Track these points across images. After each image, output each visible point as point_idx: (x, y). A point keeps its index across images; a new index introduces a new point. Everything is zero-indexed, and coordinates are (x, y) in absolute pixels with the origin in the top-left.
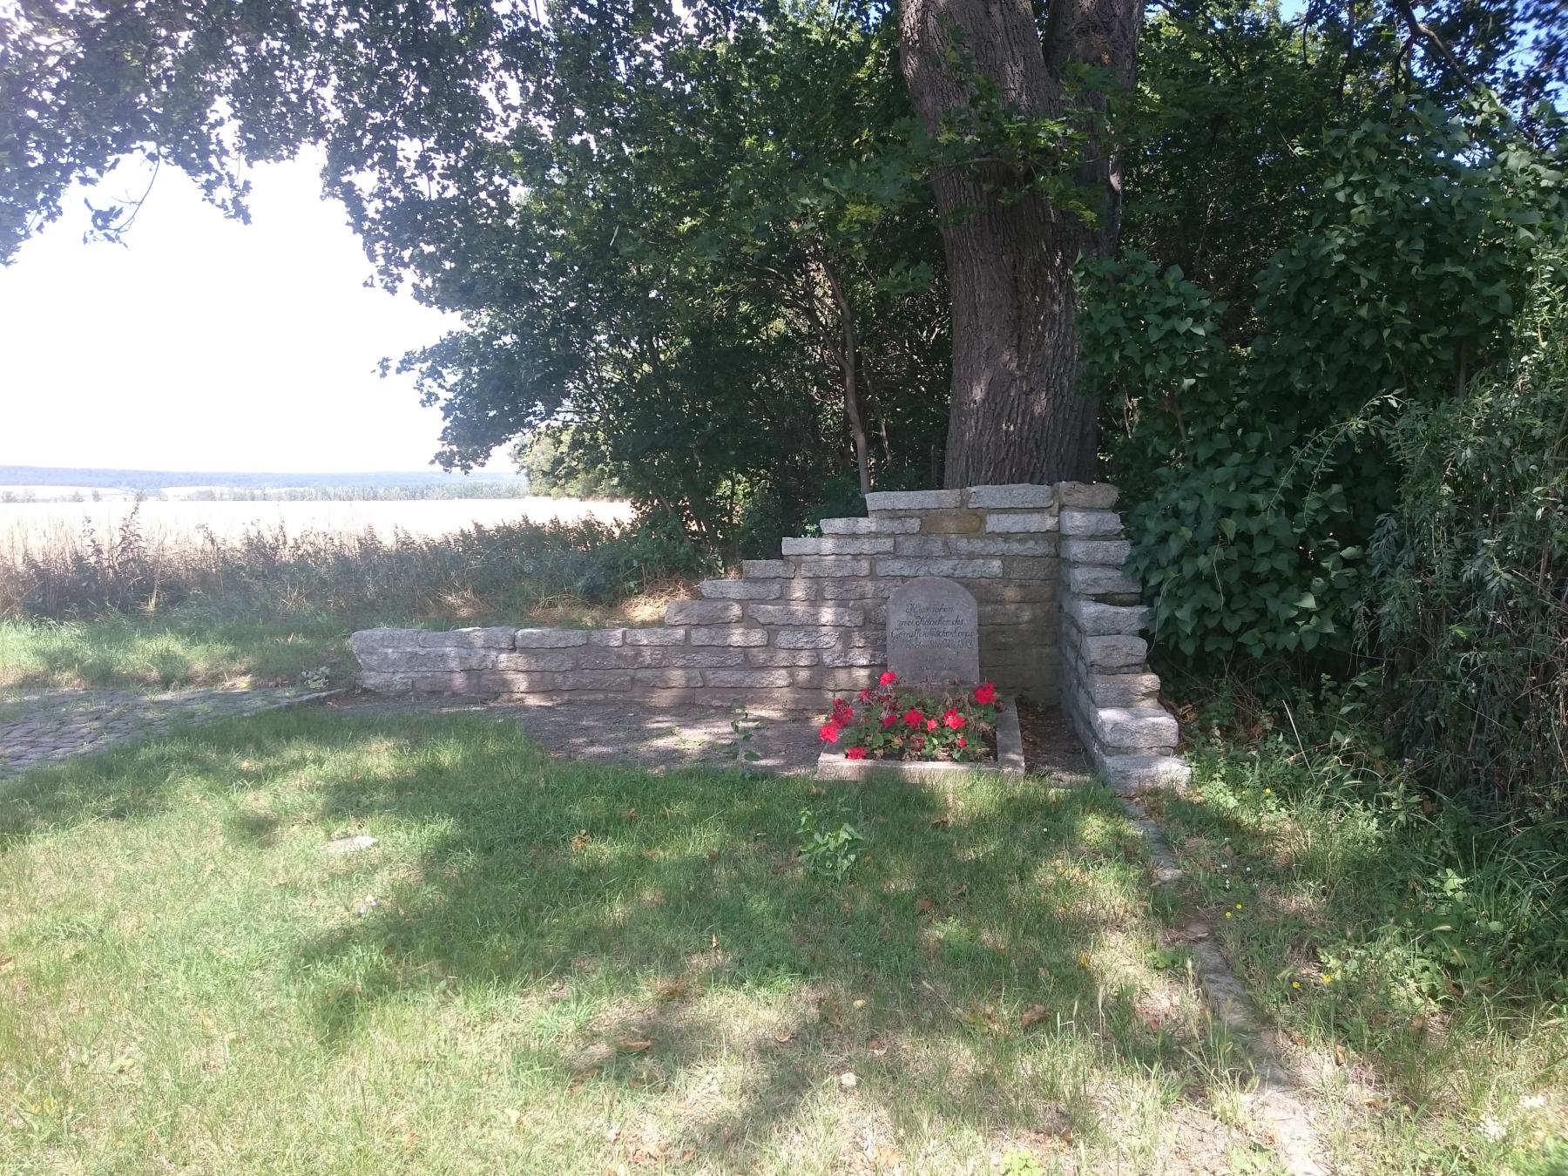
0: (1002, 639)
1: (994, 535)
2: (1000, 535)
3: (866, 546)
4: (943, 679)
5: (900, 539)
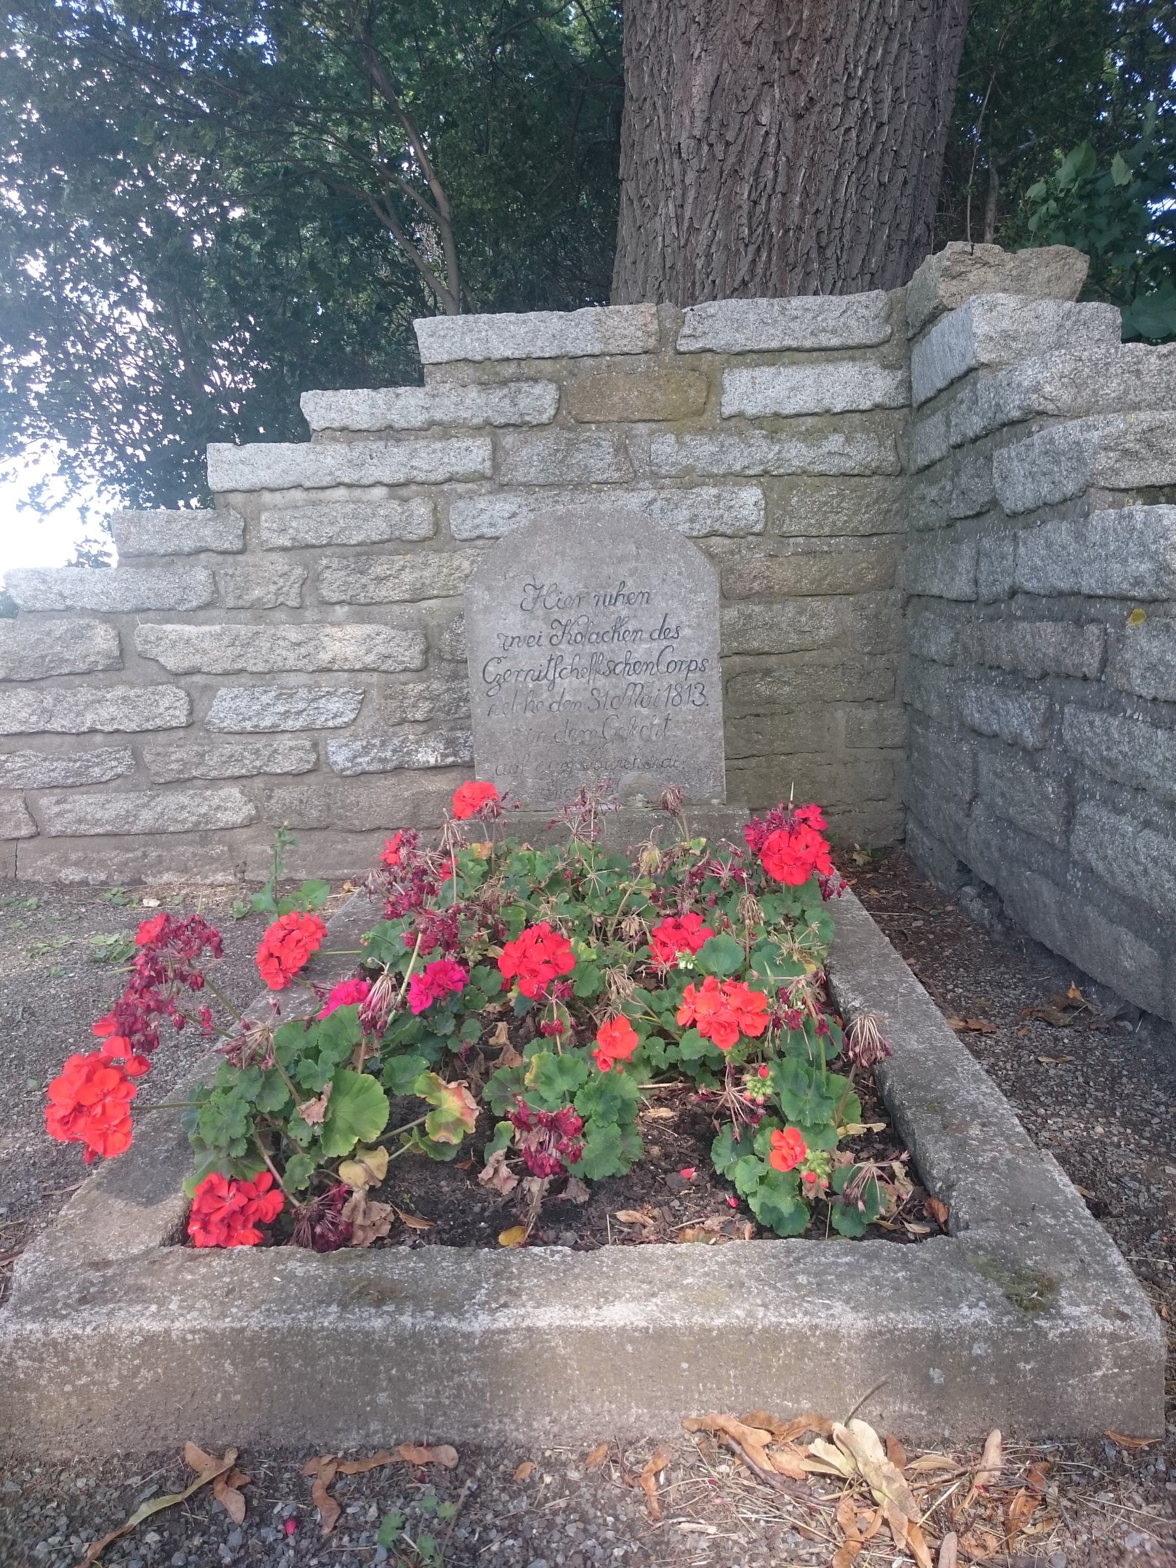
0: (763, 688)
1: (743, 424)
2: (756, 421)
4: (630, 793)
5: (509, 440)
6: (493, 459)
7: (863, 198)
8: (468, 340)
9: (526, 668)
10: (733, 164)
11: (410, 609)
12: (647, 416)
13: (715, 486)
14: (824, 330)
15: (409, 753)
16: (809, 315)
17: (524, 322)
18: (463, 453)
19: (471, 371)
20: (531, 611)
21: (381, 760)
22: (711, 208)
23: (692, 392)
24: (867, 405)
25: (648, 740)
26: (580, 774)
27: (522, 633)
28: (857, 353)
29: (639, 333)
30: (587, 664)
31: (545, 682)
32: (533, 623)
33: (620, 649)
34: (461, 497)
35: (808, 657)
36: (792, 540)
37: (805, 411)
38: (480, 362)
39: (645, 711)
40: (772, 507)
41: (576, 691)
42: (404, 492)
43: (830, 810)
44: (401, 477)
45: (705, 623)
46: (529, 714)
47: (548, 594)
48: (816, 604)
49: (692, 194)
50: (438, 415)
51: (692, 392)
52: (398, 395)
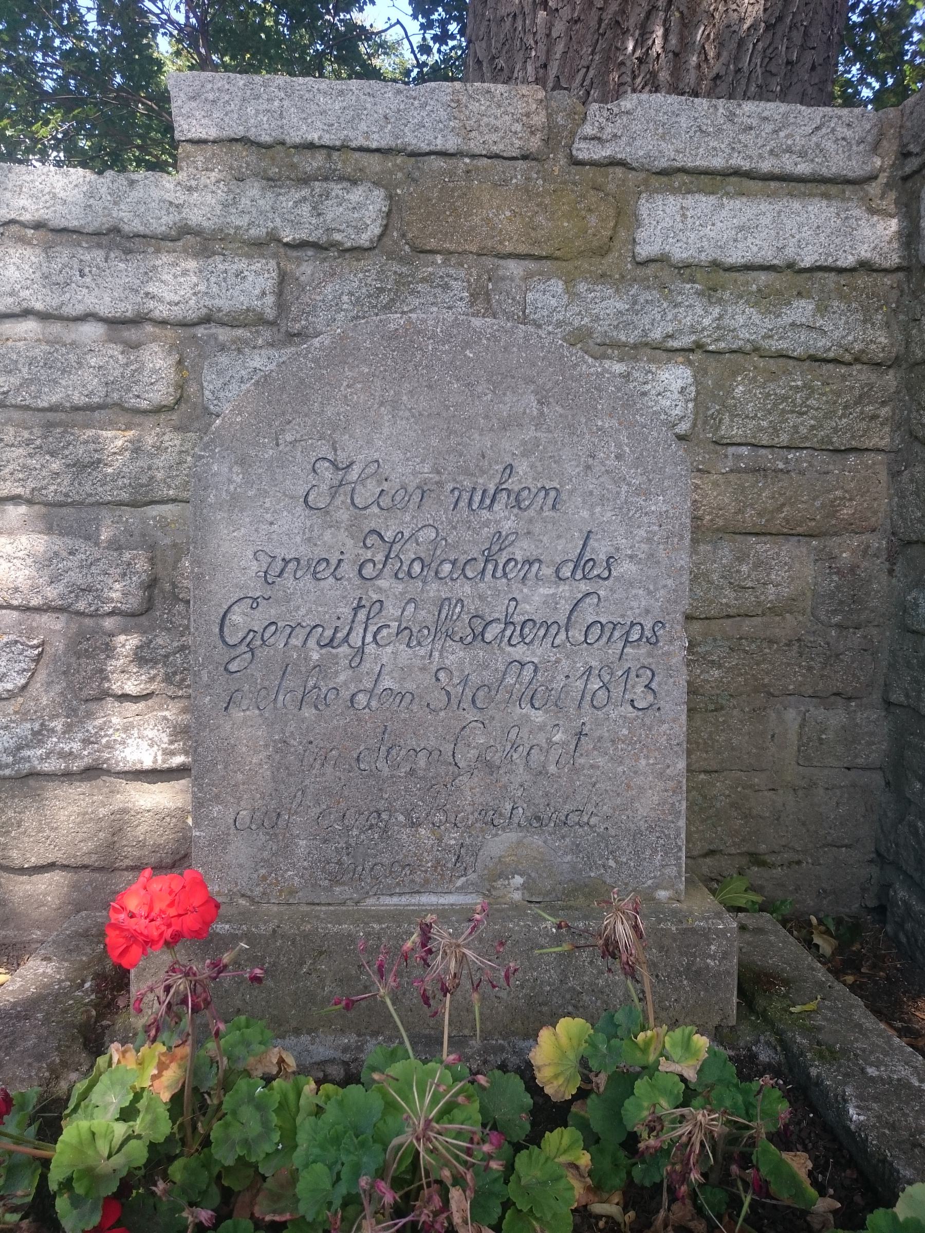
1: (666, 272)
2: (686, 270)
3: (176, 285)
4: (501, 873)
5: (307, 269)
6: (280, 294)
7: (768, 73)
8: (250, 111)
9: (309, 622)
10: (615, 13)
11: (130, 516)
12: (522, 249)
13: (621, 360)
14: (789, 150)
15: (109, 746)
16: (769, 128)
17: (341, 93)
18: (232, 280)
19: (253, 159)
20: (325, 511)
21: (62, 755)
22: (584, 63)
23: (593, 220)
24: (849, 261)
25: (542, 772)
26: (405, 835)
27: (304, 551)
28: (833, 190)
29: (518, 127)
30: (430, 621)
31: (344, 649)
32: (328, 535)
33: (497, 593)
34: (223, 348)
35: (747, 626)
36: (731, 450)
37: (758, 260)
38: (268, 147)
39: (538, 717)
40: (708, 400)
41: (405, 671)
42: (132, 334)
43: (770, 859)
44: (127, 309)
45: (661, 554)
46: (308, 712)
47: (362, 480)
48: (762, 547)
49: (560, 48)
50: (195, 217)
51: (593, 220)
52: (132, 183)
